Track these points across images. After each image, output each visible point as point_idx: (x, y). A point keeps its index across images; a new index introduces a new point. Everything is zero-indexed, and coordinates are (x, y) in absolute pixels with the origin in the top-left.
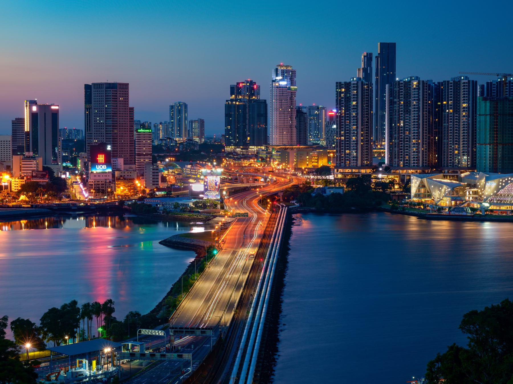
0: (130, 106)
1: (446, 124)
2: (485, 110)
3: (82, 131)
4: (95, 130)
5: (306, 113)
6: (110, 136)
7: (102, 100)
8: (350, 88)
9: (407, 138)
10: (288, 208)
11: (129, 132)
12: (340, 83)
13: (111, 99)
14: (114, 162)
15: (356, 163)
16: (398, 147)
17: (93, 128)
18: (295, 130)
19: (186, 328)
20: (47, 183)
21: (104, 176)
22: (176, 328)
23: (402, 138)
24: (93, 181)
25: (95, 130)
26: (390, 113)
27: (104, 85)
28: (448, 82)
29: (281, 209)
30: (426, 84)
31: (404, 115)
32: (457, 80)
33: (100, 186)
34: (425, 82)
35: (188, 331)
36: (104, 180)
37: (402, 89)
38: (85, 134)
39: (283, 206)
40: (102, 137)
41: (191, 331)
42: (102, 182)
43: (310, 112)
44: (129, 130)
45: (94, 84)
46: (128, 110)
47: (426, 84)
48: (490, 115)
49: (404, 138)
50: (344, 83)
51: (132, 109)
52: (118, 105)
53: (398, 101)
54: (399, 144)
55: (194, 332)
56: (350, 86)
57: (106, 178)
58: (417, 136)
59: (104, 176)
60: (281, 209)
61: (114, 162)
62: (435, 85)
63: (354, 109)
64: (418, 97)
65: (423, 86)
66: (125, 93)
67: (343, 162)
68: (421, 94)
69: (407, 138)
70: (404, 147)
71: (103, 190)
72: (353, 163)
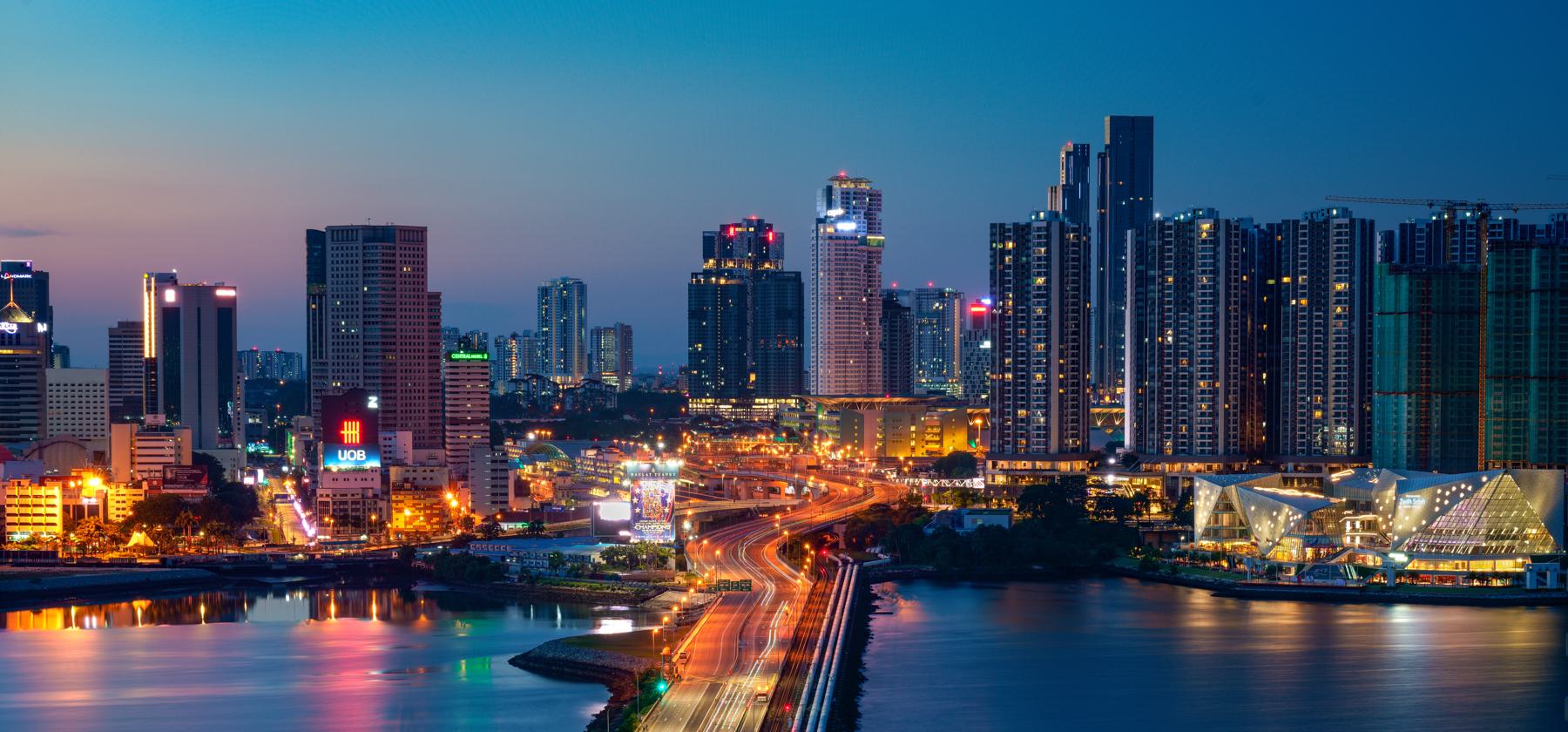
12: (1002, 226)
15: (1046, 444)
21: (359, 479)
27: (360, 232)
31: (1177, 313)
36: (360, 491)
42: (353, 495)
46: (426, 300)
50: (1011, 227)
53: (1159, 276)
59: (359, 479)
66: (416, 252)
67: (1008, 443)
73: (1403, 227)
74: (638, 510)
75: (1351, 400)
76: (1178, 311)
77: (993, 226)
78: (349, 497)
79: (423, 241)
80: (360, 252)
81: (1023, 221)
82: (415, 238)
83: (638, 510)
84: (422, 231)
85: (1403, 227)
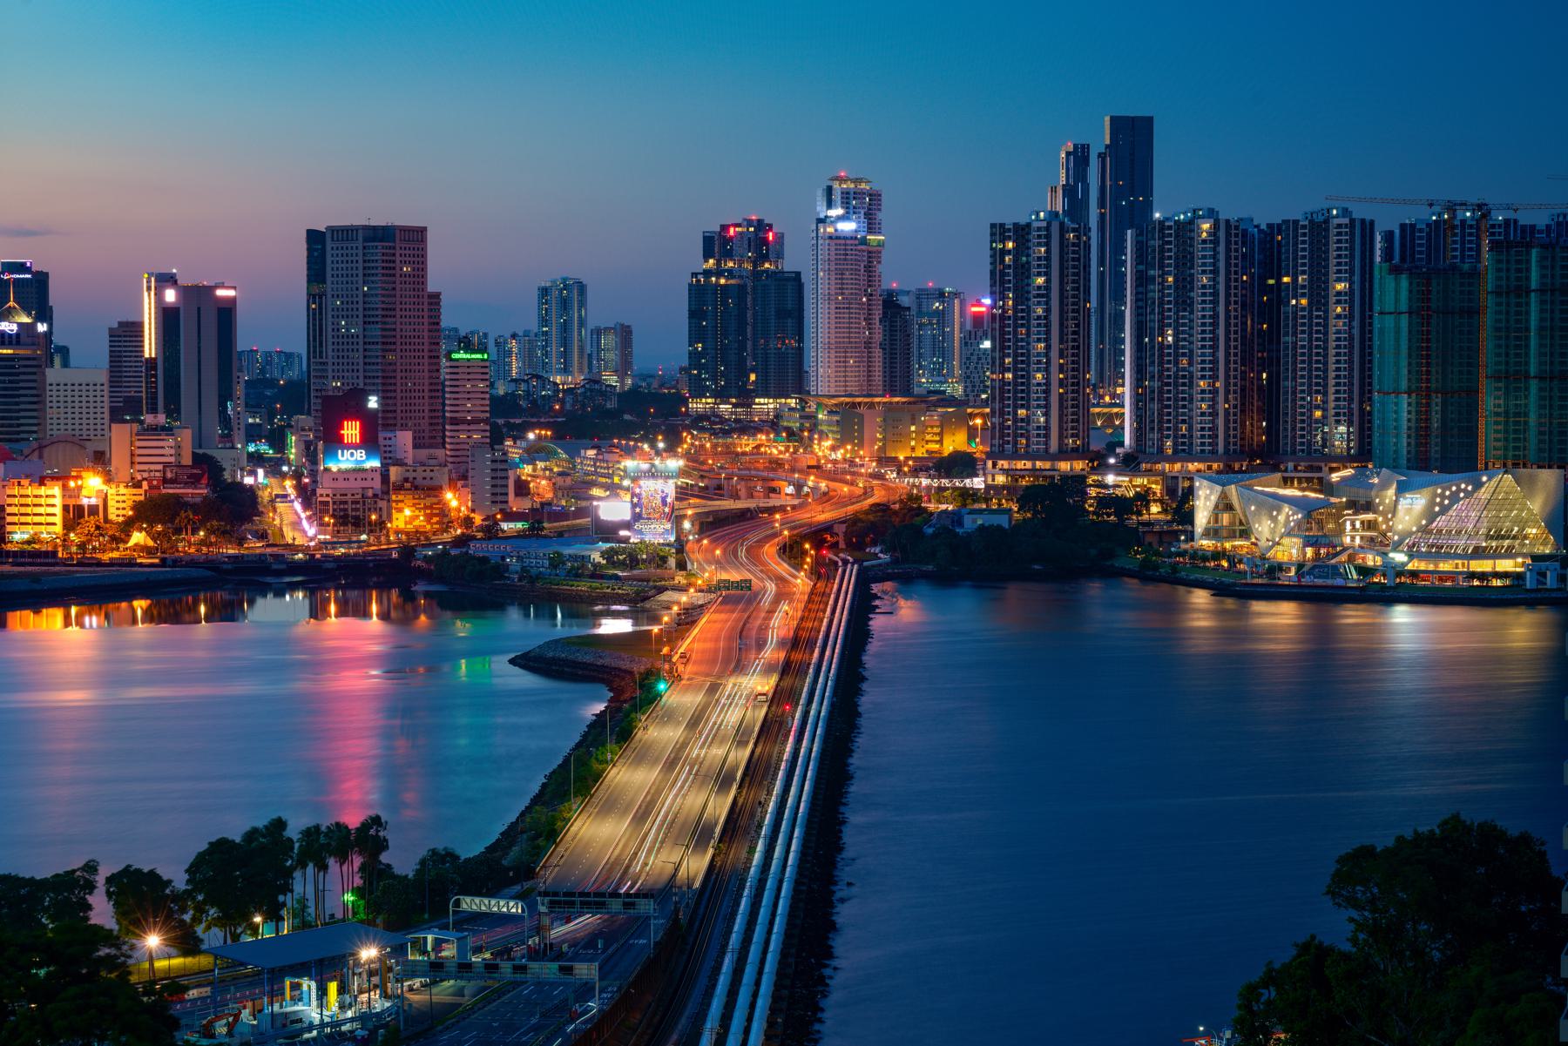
0: (431, 287)
1: (1289, 339)
3: (300, 356)
4: (336, 354)
5: (909, 309)
6: (377, 371)
10: (860, 565)
12: (1002, 225)
14: (388, 442)
16: (1161, 400)
18: (878, 354)
20: (205, 498)
22: (556, 894)
25: (336, 354)
26: (1138, 308)
28: (1296, 222)
29: (840, 570)
30: (1237, 228)
31: (1176, 313)
32: (1321, 219)
33: (349, 506)
34: (1233, 223)
37: (1169, 243)
39: (845, 562)
45: (332, 229)
47: (1237, 228)
48: (1410, 313)
49: (1176, 377)
51: (436, 297)
52: (398, 286)
54: (1161, 392)
55: (603, 904)
58: (1211, 369)
59: (359, 479)
60: (840, 570)
61: (388, 442)
62: (1261, 231)
65: (1228, 234)
69: (1184, 377)
71: (357, 518)
73: (1403, 227)
74: (638, 510)
75: (1351, 400)
76: (1178, 311)
77: (993, 226)
78: (349, 496)
79: (423, 240)
80: (360, 252)
81: (1023, 221)
82: (415, 237)
83: (638, 510)
84: (422, 231)
85: (1403, 227)
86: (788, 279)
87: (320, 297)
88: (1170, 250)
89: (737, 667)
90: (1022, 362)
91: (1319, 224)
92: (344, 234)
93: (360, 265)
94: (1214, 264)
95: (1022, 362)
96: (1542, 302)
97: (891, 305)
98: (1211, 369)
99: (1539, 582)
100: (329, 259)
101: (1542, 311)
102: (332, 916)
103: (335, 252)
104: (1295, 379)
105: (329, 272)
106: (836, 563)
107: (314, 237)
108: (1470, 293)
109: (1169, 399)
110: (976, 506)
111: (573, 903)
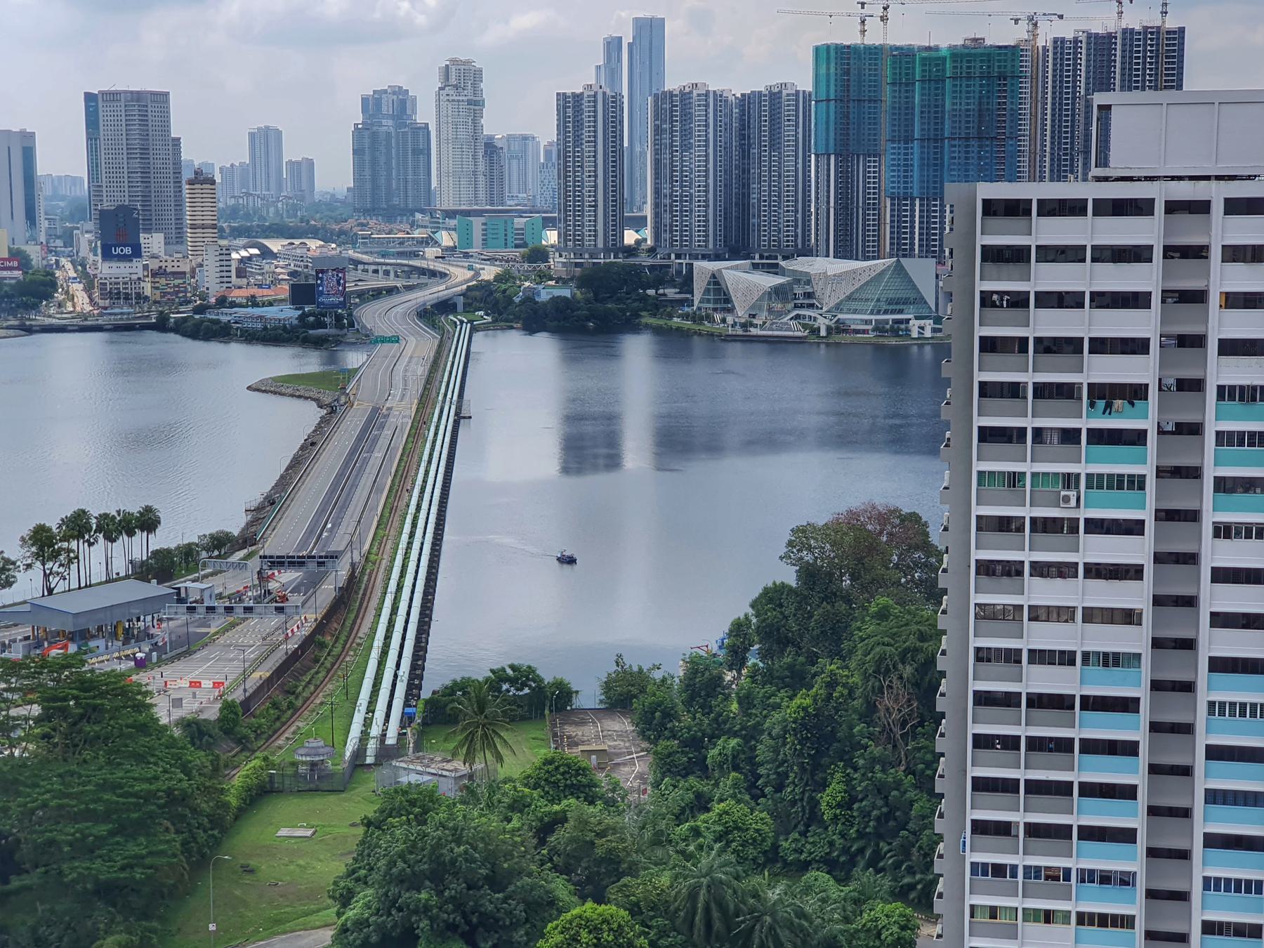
1: (755, 186)
2: (828, 91)
3: (81, 179)
4: (108, 180)
5: (502, 148)
6: (137, 192)
7: (119, 123)
8: (582, 104)
9: (686, 196)
10: (472, 324)
11: (172, 185)
12: (564, 94)
13: (139, 175)
14: (146, 241)
16: (671, 212)
17: (104, 176)
18: (481, 178)
19: (288, 557)
20: (19, 282)
22: (271, 557)
23: (676, 196)
24: (108, 276)
25: (108, 180)
26: (656, 150)
28: (760, 93)
29: (459, 327)
30: (721, 96)
32: (776, 90)
33: (121, 286)
34: (718, 93)
35: (294, 562)
37: (677, 106)
38: (89, 187)
39: (462, 322)
40: (122, 194)
41: (299, 562)
43: (509, 147)
44: (173, 227)
45: (103, 93)
47: (721, 96)
48: (836, 101)
49: (682, 196)
51: (177, 141)
52: (151, 133)
54: (671, 206)
55: (304, 563)
56: (582, 99)
57: (131, 271)
58: (704, 226)
60: (459, 327)
61: (146, 241)
62: (736, 98)
63: (589, 142)
64: (706, 156)
65: (715, 100)
68: (711, 115)
69: (686, 196)
70: (681, 211)
71: (127, 294)
72: (590, 241)
82: (161, 99)
86: (420, 128)
87: (96, 140)
88: (676, 111)
89: (378, 102)
90: (579, 216)
91: (775, 94)
92: (112, 96)
93: (123, 118)
94: (706, 156)
95: (579, 216)
96: (923, 88)
97: (491, 148)
98: (704, 226)
99: (919, 333)
100: (101, 114)
101: (923, 124)
102: (118, 574)
103: (105, 109)
104: (759, 216)
105: (101, 123)
106: (455, 323)
107: (89, 97)
108: (875, 140)
109: (677, 211)
110: (550, 283)
111: (283, 562)
